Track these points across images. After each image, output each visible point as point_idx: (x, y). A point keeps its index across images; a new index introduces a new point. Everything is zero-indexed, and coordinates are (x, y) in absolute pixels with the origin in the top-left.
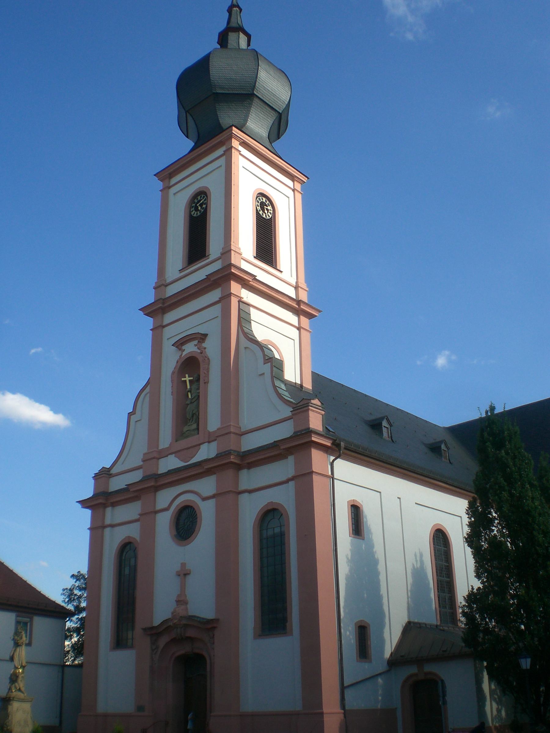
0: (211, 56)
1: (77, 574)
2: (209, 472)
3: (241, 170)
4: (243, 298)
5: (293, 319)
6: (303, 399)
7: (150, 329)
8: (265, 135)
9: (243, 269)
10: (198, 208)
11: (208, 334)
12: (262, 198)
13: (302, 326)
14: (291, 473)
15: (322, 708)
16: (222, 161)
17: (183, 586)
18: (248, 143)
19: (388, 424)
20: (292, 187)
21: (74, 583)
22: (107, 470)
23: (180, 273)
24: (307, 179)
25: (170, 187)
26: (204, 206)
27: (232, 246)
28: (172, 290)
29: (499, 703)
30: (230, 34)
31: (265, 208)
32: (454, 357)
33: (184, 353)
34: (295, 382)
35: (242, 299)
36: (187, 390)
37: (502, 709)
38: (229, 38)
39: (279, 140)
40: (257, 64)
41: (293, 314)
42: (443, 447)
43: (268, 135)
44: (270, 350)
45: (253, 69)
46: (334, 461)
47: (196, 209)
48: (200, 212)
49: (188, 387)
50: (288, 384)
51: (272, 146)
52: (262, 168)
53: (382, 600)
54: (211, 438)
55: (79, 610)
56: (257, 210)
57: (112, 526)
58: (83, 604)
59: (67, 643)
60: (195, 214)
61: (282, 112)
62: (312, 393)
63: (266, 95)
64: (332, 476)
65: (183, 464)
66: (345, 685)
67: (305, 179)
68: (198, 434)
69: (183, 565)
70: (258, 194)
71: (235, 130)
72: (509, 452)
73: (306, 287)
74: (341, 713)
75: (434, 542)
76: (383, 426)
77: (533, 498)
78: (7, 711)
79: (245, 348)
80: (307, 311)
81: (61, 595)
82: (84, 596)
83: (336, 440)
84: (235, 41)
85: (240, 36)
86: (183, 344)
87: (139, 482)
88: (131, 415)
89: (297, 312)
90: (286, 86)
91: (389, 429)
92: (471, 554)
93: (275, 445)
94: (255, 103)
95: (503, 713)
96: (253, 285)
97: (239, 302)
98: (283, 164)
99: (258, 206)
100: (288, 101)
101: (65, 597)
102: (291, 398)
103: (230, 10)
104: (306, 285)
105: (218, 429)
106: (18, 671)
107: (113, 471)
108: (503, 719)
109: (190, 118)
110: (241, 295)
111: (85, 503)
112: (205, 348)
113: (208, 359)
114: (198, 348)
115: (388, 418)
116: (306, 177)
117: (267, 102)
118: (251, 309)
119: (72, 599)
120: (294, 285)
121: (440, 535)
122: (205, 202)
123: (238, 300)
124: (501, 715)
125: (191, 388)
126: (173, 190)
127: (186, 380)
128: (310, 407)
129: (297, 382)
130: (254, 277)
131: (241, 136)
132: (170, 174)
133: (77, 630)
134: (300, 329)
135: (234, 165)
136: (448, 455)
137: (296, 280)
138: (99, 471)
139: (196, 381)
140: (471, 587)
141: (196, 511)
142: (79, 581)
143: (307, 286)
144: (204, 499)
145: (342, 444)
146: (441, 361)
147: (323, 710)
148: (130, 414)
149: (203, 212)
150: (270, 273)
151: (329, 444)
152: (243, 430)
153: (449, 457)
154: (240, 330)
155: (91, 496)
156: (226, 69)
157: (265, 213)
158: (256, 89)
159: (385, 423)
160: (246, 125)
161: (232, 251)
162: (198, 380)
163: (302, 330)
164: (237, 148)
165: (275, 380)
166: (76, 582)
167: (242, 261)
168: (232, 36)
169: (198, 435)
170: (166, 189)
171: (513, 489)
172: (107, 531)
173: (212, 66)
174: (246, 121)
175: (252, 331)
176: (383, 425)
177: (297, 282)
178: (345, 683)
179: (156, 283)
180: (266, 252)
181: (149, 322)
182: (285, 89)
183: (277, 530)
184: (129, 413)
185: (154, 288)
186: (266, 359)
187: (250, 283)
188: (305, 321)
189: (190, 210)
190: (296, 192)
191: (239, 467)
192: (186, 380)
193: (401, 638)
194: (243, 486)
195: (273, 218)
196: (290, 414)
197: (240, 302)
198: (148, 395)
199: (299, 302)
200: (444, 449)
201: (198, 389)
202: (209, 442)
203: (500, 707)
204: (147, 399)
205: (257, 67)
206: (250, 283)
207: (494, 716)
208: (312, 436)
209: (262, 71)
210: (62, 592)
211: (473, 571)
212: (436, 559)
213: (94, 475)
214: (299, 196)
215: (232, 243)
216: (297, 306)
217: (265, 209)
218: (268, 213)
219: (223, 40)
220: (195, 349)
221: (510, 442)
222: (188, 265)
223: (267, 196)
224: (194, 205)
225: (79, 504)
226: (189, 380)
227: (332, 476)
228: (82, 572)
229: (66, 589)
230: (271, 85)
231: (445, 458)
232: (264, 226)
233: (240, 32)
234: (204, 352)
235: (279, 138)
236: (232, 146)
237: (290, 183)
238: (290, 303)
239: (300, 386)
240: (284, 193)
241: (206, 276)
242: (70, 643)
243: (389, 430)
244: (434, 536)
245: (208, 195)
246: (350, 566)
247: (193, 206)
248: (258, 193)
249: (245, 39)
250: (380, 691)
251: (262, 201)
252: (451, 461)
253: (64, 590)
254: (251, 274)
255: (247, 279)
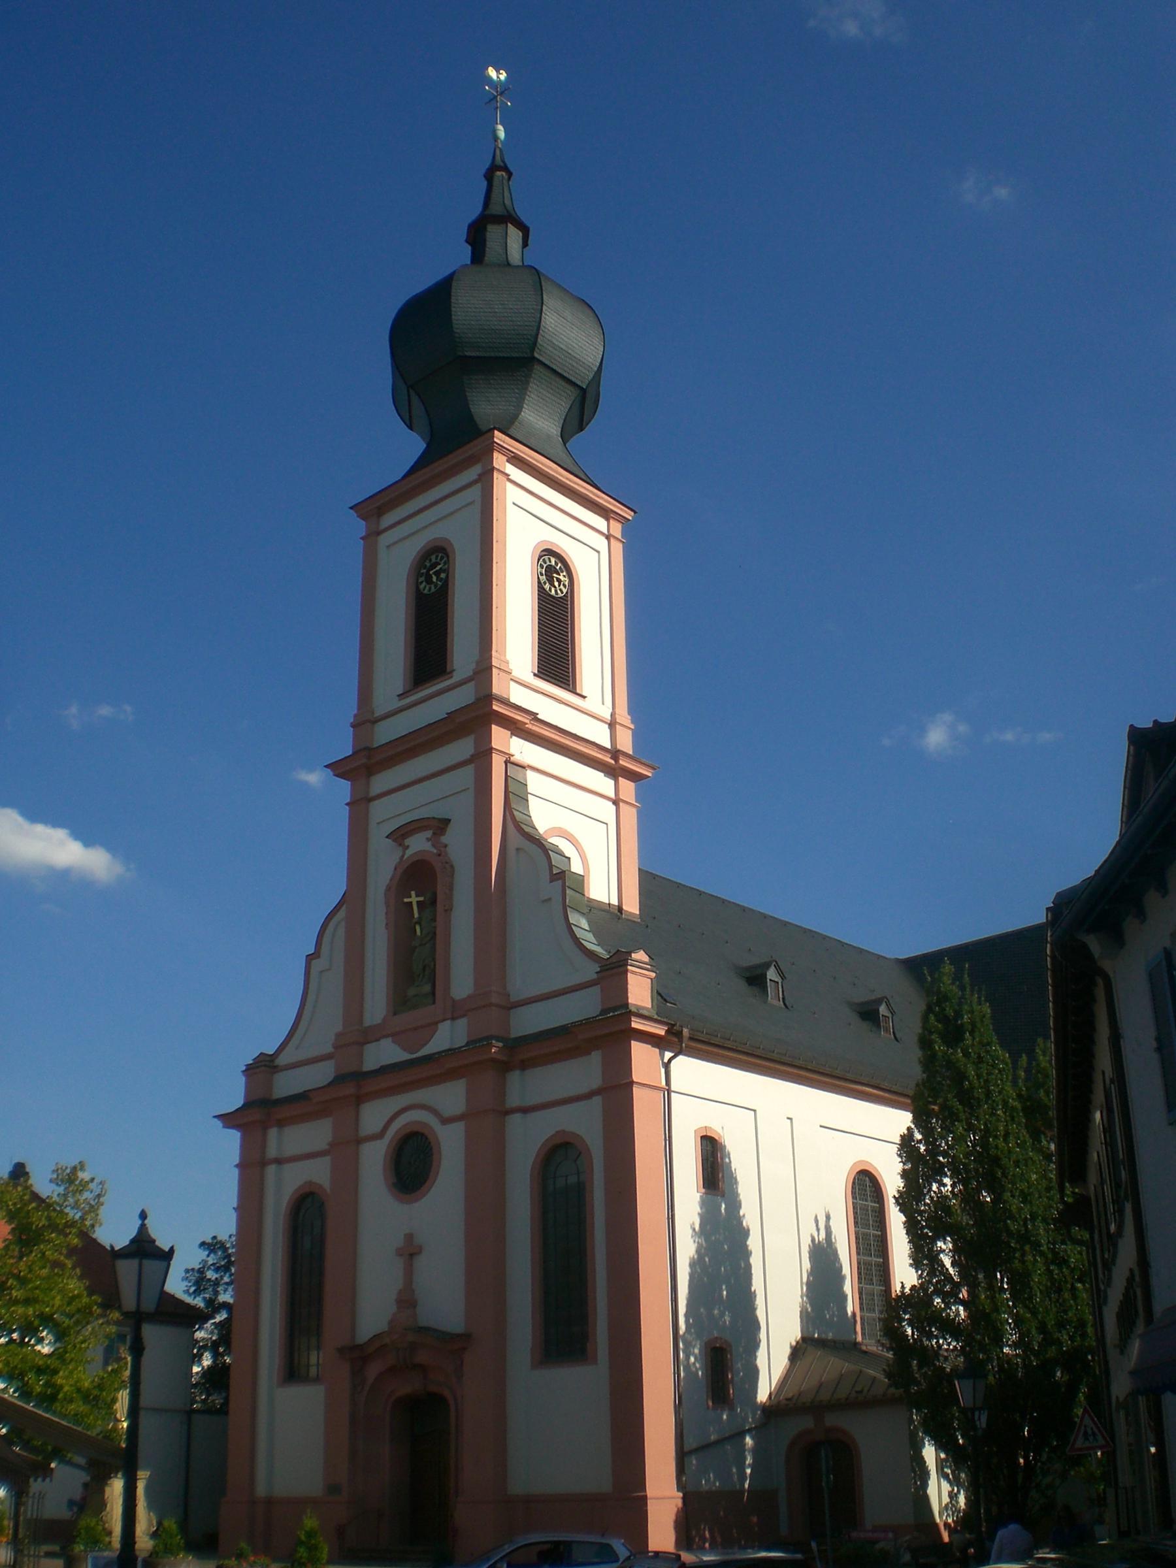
0: (455, 278)
1: (210, 1241)
2: (452, 1074)
3: (511, 510)
4: (513, 756)
5: (606, 785)
6: (618, 950)
7: (346, 802)
8: (555, 432)
9: (514, 704)
10: (432, 577)
11: (450, 820)
12: (549, 559)
13: (621, 797)
14: (596, 1082)
15: (644, 1489)
16: (475, 493)
17: (409, 1272)
18: (523, 457)
19: (778, 975)
20: (606, 532)
21: (204, 1257)
22: (268, 1058)
23: (400, 700)
24: (632, 513)
25: (379, 533)
26: (443, 576)
27: (493, 659)
28: (386, 733)
29: (955, 1482)
30: (490, 228)
31: (554, 577)
32: (962, 728)
33: (409, 853)
34: (608, 902)
35: (512, 758)
36: (414, 921)
37: (959, 1491)
38: (488, 235)
39: (582, 433)
40: (541, 302)
41: (605, 776)
42: (883, 1009)
43: (562, 431)
44: (561, 855)
45: (533, 311)
46: (670, 1060)
47: (429, 580)
48: (436, 586)
49: (416, 915)
50: (594, 910)
51: (567, 449)
52: (548, 502)
53: (755, 1300)
54: (456, 1011)
55: (214, 1306)
56: (539, 582)
57: (279, 1161)
58: (226, 1297)
59: (196, 1369)
60: (425, 589)
61: (587, 387)
62: (639, 920)
63: (557, 358)
64: (667, 1088)
65: (405, 1056)
66: (686, 1449)
67: (629, 515)
68: (434, 1003)
69: (409, 1237)
70: (542, 551)
71: (499, 437)
72: (970, 1053)
73: (630, 721)
74: (678, 1498)
75: (853, 1193)
76: (768, 980)
77: (1006, 1135)
78: (104, 1496)
79: (518, 849)
80: (632, 770)
81: (183, 1280)
82: (223, 1282)
83: (673, 1025)
84: (500, 242)
85: (509, 231)
86: (405, 836)
87: (330, 1084)
88: (312, 959)
89: (613, 772)
90: (595, 336)
91: (780, 984)
92: (903, 1227)
93: (563, 1031)
94: (535, 374)
95: (962, 1500)
96: (531, 729)
97: (506, 762)
98: (588, 490)
99: (542, 575)
100: (598, 364)
101: (190, 1284)
102: (598, 945)
103: (489, 176)
104: (629, 717)
105: (469, 997)
106: (121, 1427)
107: (282, 1060)
108: (962, 1511)
109: (415, 400)
110: (509, 750)
111: (228, 1120)
112: (446, 846)
113: (452, 867)
114: (433, 846)
115: (777, 964)
116: (632, 510)
117: (560, 371)
118: (529, 773)
119: (202, 1288)
120: (608, 720)
121: (865, 1181)
122: (444, 568)
123: (505, 759)
124: (957, 1502)
125: (420, 918)
126: (384, 539)
127: (411, 902)
128: (629, 967)
129: (612, 902)
130: (534, 716)
131: (512, 446)
132: (379, 508)
133: (214, 1347)
134: (619, 804)
135: (497, 503)
136: (893, 1025)
137: (611, 710)
138: (253, 1060)
139: (430, 904)
140: (901, 1285)
141: (430, 1143)
142: (215, 1255)
143: (631, 720)
144: (446, 1121)
145: (686, 1031)
146: (936, 737)
147: (646, 1491)
148: (310, 958)
149: (441, 587)
150: (564, 701)
151: (662, 1033)
152: (513, 999)
153: (893, 1029)
154: (508, 817)
155: (240, 1106)
156: (481, 310)
157: (555, 587)
158: (538, 348)
159: (771, 974)
160: (520, 416)
161: (494, 669)
162: (434, 902)
163: (621, 804)
164: (503, 470)
165: (570, 911)
166: (208, 1256)
167: (512, 683)
168: (493, 231)
169: (433, 1006)
170: (372, 536)
171: (973, 1118)
172: (271, 1170)
173: (455, 305)
174: (519, 408)
175: (530, 817)
176: (769, 977)
177: (613, 715)
178: (685, 1446)
179: (355, 716)
180: (557, 618)
181: (344, 788)
182: (593, 342)
183: (572, 1180)
184: (308, 956)
185: (353, 726)
186: (554, 873)
187: (527, 726)
188: (628, 788)
189: (418, 580)
190: (612, 540)
191: (504, 1067)
192: (411, 902)
193: (788, 1367)
194: (513, 1101)
195: (569, 594)
196: (595, 976)
197: (508, 764)
198: (343, 924)
199: (615, 753)
200: (884, 1014)
201: (434, 920)
202: (453, 1019)
203: (956, 1489)
204: (341, 931)
205: (540, 307)
206: (527, 726)
207: (943, 1505)
208: (631, 1021)
209: (548, 314)
210: (184, 1274)
211: (907, 1255)
212: (856, 1223)
213: (244, 1068)
214: (618, 548)
215: (494, 653)
216: (613, 762)
217: (555, 579)
218: (559, 586)
219: (476, 236)
220: (427, 846)
221: (972, 1033)
222: (414, 686)
223: (558, 554)
224: (425, 571)
225: (219, 1120)
226: (417, 902)
227: (667, 1088)
228: (219, 1238)
229: (193, 1270)
230: (565, 338)
231: (887, 1030)
232: (552, 635)
233: (509, 225)
234: (443, 854)
235: (581, 429)
236: (494, 467)
237: (600, 523)
238: (600, 756)
239: (617, 907)
240: (590, 545)
241: (447, 714)
242: (200, 1369)
243: (780, 987)
244: (854, 1183)
245: (450, 555)
246: (698, 1243)
247: (423, 573)
248: (542, 549)
249: (519, 237)
250: (749, 1458)
251: (548, 563)
252: (897, 1036)
253: (187, 1271)
254: (528, 711)
255: (520, 721)
